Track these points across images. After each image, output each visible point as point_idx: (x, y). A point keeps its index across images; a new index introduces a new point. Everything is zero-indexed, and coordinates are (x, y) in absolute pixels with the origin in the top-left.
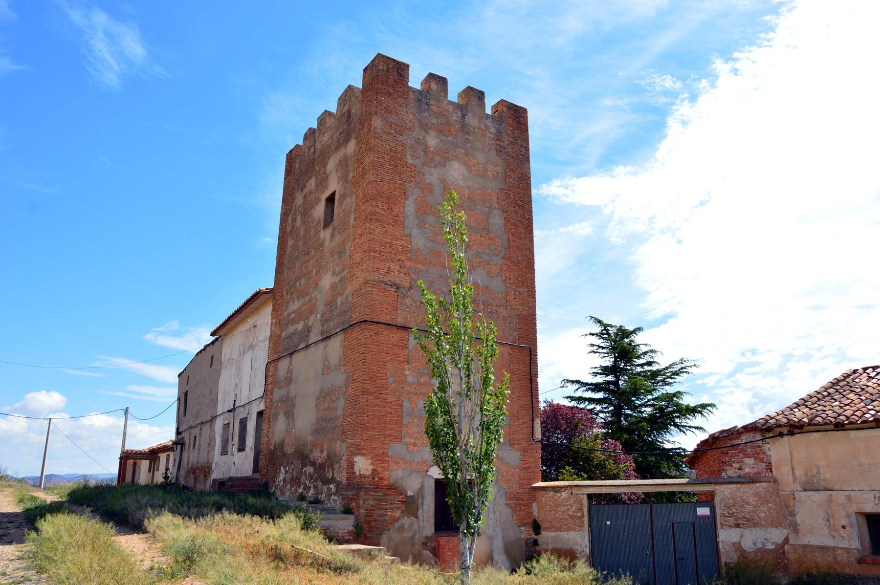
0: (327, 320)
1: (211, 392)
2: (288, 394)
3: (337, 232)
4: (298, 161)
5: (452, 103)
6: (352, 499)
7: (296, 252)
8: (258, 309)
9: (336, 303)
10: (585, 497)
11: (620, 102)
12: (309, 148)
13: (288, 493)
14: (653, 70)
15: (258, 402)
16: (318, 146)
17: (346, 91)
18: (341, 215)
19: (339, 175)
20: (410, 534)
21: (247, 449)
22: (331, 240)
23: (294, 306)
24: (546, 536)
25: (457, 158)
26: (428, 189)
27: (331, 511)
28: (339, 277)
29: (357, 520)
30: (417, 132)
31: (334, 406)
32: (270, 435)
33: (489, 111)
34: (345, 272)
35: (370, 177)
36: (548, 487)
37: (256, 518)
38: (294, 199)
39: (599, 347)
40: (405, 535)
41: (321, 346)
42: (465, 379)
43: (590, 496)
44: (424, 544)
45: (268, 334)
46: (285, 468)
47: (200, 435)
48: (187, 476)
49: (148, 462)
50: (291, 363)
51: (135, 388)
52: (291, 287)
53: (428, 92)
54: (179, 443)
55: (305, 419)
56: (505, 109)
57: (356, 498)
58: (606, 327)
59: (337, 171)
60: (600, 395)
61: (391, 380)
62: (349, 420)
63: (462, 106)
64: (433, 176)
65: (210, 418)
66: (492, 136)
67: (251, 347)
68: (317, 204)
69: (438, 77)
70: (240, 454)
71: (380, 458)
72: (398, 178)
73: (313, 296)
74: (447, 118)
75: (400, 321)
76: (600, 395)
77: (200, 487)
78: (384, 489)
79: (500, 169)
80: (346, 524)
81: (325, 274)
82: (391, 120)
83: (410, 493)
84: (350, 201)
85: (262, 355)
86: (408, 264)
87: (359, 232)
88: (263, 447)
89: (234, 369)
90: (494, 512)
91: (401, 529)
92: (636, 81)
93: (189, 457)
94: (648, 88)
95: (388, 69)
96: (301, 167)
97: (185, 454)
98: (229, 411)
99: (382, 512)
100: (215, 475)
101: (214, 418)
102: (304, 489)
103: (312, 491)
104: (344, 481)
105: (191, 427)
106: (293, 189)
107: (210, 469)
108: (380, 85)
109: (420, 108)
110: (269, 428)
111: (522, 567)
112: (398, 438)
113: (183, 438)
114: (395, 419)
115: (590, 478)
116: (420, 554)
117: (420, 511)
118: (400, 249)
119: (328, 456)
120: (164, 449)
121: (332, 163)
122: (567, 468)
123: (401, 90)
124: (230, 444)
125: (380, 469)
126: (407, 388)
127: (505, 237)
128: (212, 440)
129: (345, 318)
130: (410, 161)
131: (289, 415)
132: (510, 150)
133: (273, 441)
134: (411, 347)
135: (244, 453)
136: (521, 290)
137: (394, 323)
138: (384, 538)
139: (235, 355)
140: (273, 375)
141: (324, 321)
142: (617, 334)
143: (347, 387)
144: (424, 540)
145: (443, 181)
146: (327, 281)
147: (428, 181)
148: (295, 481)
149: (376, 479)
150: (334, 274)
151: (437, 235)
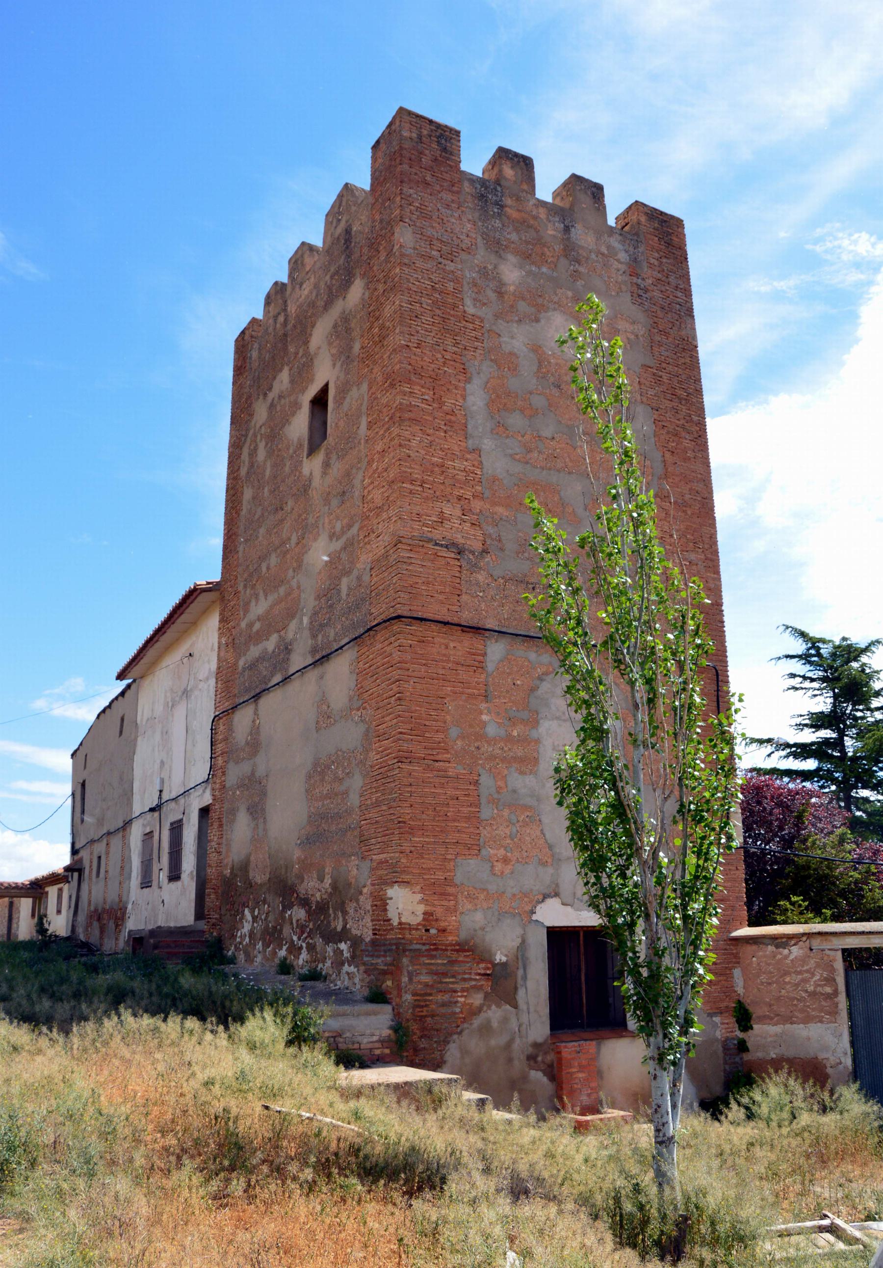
0: (322, 626)
1: (121, 779)
3: (334, 457)
4: (256, 346)
5: (543, 204)
6: (385, 973)
7: (259, 510)
8: (194, 624)
9: (339, 591)
10: (839, 955)
11: (781, 285)
12: (276, 318)
13: (259, 959)
14: (838, 225)
15: (200, 790)
16: (292, 308)
17: (340, 196)
18: (342, 424)
19: (334, 351)
20: (502, 1040)
21: (185, 876)
22: (324, 473)
23: (259, 608)
24: (765, 1035)
25: (559, 306)
26: (507, 362)
27: (343, 997)
29: (397, 1014)
30: (481, 255)
31: (342, 788)
33: (611, 221)
34: (354, 530)
35: (397, 339)
36: (763, 937)
37: (192, 1023)
38: (251, 415)
39: (804, 678)
40: (493, 1042)
41: (312, 675)
42: (643, 709)
43: (847, 953)
44: (531, 1058)
45: (214, 666)
46: (252, 912)
47: (107, 853)
48: (89, 925)
49: (30, 900)
50: (256, 713)
51: (23, 785)
52: (251, 575)
53: (498, 182)
54: (74, 869)
55: (288, 815)
56: (643, 219)
57: (394, 970)
58: (814, 643)
59: (330, 344)
60: (811, 764)
61: (454, 732)
62: (373, 814)
63: (562, 209)
64: (516, 339)
65: (121, 824)
66: (623, 267)
68: (293, 414)
69: (516, 155)
71: (439, 890)
72: (449, 341)
74: (537, 231)
75: (466, 617)
76: (811, 764)
77: (109, 945)
78: (448, 952)
79: (641, 330)
80: (373, 1025)
81: (315, 539)
82: (429, 232)
83: (500, 958)
84: (358, 394)
85: (204, 704)
86: (477, 505)
87: (379, 448)
88: (211, 872)
89: (158, 736)
91: (486, 1030)
92: (809, 247)
93: (90, 892)
94: (829, 257)
95: (420, 137)
96: (260, 357)
97: (85, 887)
98: (152, 810)
99: (446, 997)
100: (134, 923)
101: (128, 824)
102: (289, 951)
103: (304, 956)
104: (368, 936)
105: (92, 842)
106: (249, 397)
107: (124, 914)
108: (406, 167)
109: (484, 210)
110: (221, 837)
111: (734, 1105)
112: (474, 848)
113: (81, 860)
114: (465, 810)
115: (837, 918)
116: (525, 1078)
117: (521, 993)
118: (461, 476)
119: (335, 886)
120: (53, 879)
121: (319, 335)
122: (794, 899)
123: (447, 176)
125: (439, 912)
126: (486, 748)
127: (658, 455)
128: (125, 861)
129: (357, 616)
130: (471, 310)
131: (257, 811)
132: (657, 294)
133: (228, 861)
134: (490, 666)
135: (179, 883)
136: (692, 556)
137: (455, 620)
138: (452, 1052)
139: (159, 709)
140: (226, 739)
141: (316, 629)
142: (834, 655)
143: (366, 751)
144: (530, 1050)
145: (536, 349)
146: (320, 554)
147: (507, 348)
148: (272, 935)
149: (433, 931)
150: (332, 536)
151: (530, 451)
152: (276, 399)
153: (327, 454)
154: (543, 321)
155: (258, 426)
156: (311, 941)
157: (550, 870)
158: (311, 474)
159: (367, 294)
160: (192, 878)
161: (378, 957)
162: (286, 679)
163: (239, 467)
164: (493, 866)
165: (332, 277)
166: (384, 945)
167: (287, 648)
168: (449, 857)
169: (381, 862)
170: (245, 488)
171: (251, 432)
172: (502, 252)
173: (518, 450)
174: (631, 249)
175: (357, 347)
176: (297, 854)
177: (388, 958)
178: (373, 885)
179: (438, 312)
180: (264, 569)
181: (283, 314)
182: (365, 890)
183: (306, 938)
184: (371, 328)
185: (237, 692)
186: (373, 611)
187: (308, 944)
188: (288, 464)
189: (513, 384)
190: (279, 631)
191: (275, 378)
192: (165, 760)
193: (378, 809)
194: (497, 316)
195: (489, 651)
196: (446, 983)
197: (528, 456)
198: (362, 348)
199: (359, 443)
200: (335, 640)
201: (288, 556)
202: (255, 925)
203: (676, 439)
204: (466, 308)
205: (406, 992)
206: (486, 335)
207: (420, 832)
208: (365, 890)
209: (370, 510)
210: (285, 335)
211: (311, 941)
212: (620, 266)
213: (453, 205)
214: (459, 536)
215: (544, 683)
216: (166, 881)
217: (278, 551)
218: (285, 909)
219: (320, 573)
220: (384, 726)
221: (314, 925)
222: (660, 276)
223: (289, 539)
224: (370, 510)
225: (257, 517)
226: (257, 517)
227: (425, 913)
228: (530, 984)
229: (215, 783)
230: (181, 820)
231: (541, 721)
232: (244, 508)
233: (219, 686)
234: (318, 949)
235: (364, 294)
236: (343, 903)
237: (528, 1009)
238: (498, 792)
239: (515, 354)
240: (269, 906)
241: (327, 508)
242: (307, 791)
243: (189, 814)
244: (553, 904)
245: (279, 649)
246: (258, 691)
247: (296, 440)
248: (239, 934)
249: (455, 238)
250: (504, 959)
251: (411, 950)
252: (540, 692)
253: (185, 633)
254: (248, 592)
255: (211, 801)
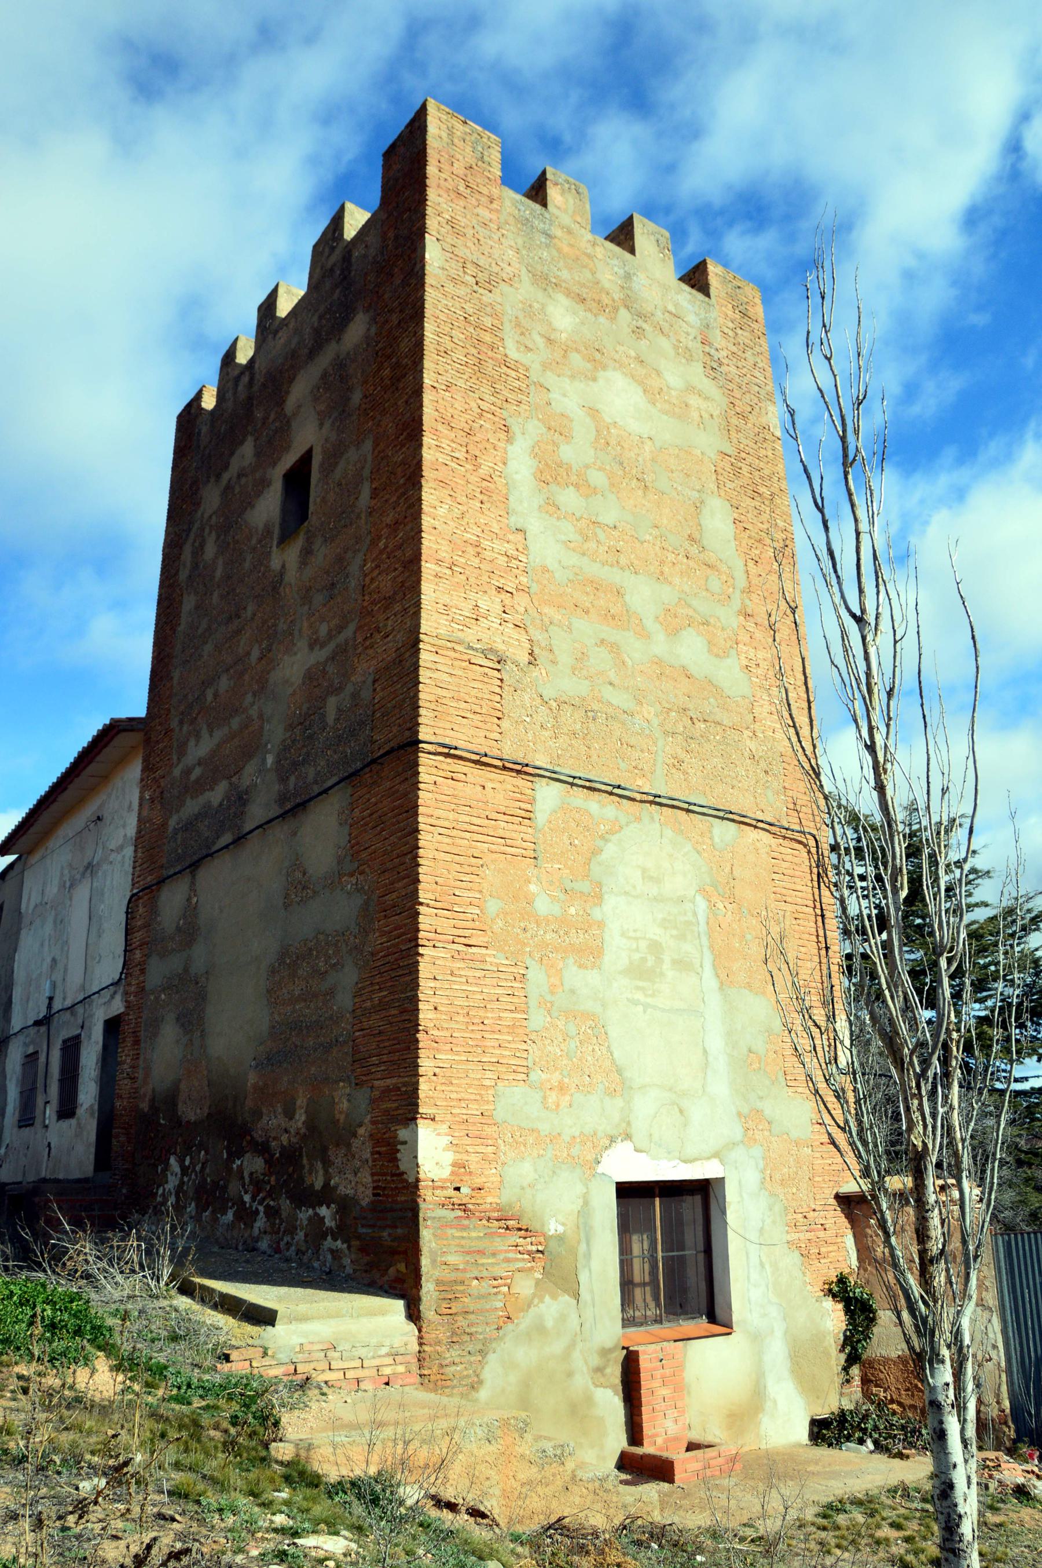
0: (295, 765)
2: (186, 970)
3: (319, 541)
8: (105, 778)
20: (557, 1347)
21: (81, 1111)
23: (200, 749)
26: (559, 428)
28: (332, 646)
30: (525, 290)
32: (140, 1074)
41: (279, 832)
45: (131, 830)
46: (181, 1161)
59: (316, 399)
61: (493, 906)
64: (567, 396)
66: (693, 332)
67: (90, 869)
68: (259, 494)
70: (65, 1124)
73: (253, 712)
75: (509, 750)
82: (462, 252)
85: (117, 881)
87: (389, 520)
90: (762, 1264)
98: (37, 1023)
102: (238, 1217)
104: (366, 1197)
110: (137, 1057)
117: (583, 1278)
119: (311, 1126)
124: (40, 1101)
130: (513, 353)
131: (192, 1021)
135: (73, 1122)
139: (52, 890)
140: (147, 926)
145: (593, 412)
146: (293, 666)
151: (586, 539)
152: (234, 480)
153: (308, 539)
154: (601, 382)
155: (206, 516)
156: (272, 1203)
157: (619, 1102)
158: (283, 566)
159: (373, 330)
160: (92, 1114)
161: (383, 1228)
162: (239, 839)
163: (178, 571)
164: (545, 1098)
165: (321, 318)
166: (392, 1210)
167: (240, 798)
168: (487, 1083)
169: (387, 1091)
170: (185, 596)
171: (197, 525)
172: (550, 290)
173: (572, 537)
174: (702, 312)
175: (357, 397)
176: (252, 1078)
177: (399, 1231)
178: (373, 1123)
179: (474, 351)
180: (210, 697)
181: (247, 373)
182: (361, 1131)
183: (264, 1199)
184: (379, 370)
185: (164, 861)
186: (376, 737)
187: (268, 1207)
188: (249, 557)
189: (566, 453)
190: (229, 777)
191: (232, 454)
192: (58, 958)
193: (384, 1013)
194: (545, 366)
195: (539, 795)
196: (483, 1265)
197: (586, 546)
198: (365, 397)
199: (359, 517)
200: (316, 782)
201: (246, 677)
202: (186, 1179)
203: (760, 546)
204: (508, 352)
205: (427, 1281)
206: (532, 388)
207: (448, 1047)
208: (361, 1131)
209: (374, 603)
210: (250, 398)
211: (272, 1203)
212: (690, 330)
213: (492, 225)
214: (499, 640)
215: (610, 844)
216: (54, 1117)
217: (232, 671)
218: (233, 1155)
219: (294, 694)
220: (394, 895)
221: (277, 1180)
222: (734, 349)
223: (248, 654)
224: (374, 603)
225: (200, 631)
226: (200, 631)
227: (454, 1165)
228: (595, 1264)
229: (129, 984)
230: (78, 1036)
231: (606, 897)
232: (183, 621)
233: (140, 855)
234: (284, 1215)
235: (369, 330)
236: (325, 1149)
237: (593, 1299)
238: (552, 993)
239: (567, 417)
240: (207, 1153)
241: (306, 607)
242: (268, 991)
243: (90, 1029)
244: (623, 1148)
245: (229, 800)
246: (195, 858)
247: (261, 526)
248: (160, 1191)
249: (494, 265)
250: (561, 1229)
251: (434, 1218)
252: (604, 856)
253: (92, 790)
254: (185, 728)
255: (122, 1010)
